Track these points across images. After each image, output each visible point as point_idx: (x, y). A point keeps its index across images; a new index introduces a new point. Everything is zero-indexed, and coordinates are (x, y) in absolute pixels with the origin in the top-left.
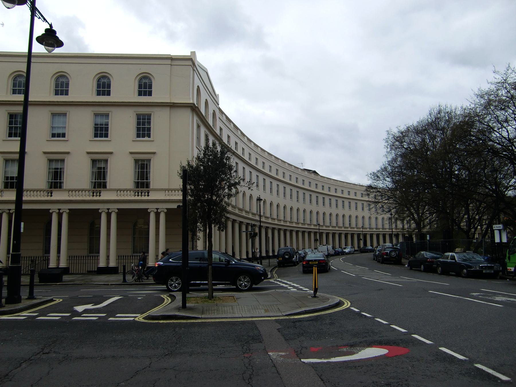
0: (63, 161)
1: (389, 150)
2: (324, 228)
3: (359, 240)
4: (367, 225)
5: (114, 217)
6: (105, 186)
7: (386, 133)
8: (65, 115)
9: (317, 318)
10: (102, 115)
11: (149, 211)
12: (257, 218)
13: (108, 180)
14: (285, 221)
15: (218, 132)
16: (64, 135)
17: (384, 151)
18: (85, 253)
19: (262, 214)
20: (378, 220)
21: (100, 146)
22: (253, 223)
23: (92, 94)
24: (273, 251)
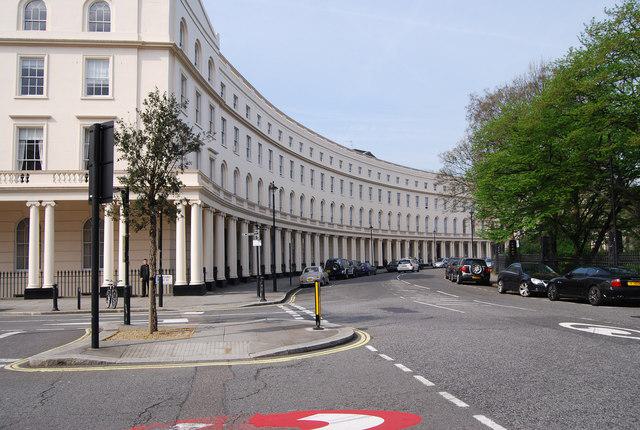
0: (40, 129)
1: (473, 122)
2: (380, 232)
3: (420, 248)
4: (441, 230)
5: (48, 213)
6: (39, 167)
7: (469, 99)
8: (106, 61)
9: (300, 363)
10: (33, 59)
11: (28, 205)
12: (268, 214)
13: (43, 158)
14: (322, 222)
15: (218, 90)
16: (106, 91)
17: (466, 124)
18: (10, 268)
19: (277, 208)
20: (454, 222)
21: (31, 107)
22: (315, 231)
23: (83, 30)
24: (273, 267)
